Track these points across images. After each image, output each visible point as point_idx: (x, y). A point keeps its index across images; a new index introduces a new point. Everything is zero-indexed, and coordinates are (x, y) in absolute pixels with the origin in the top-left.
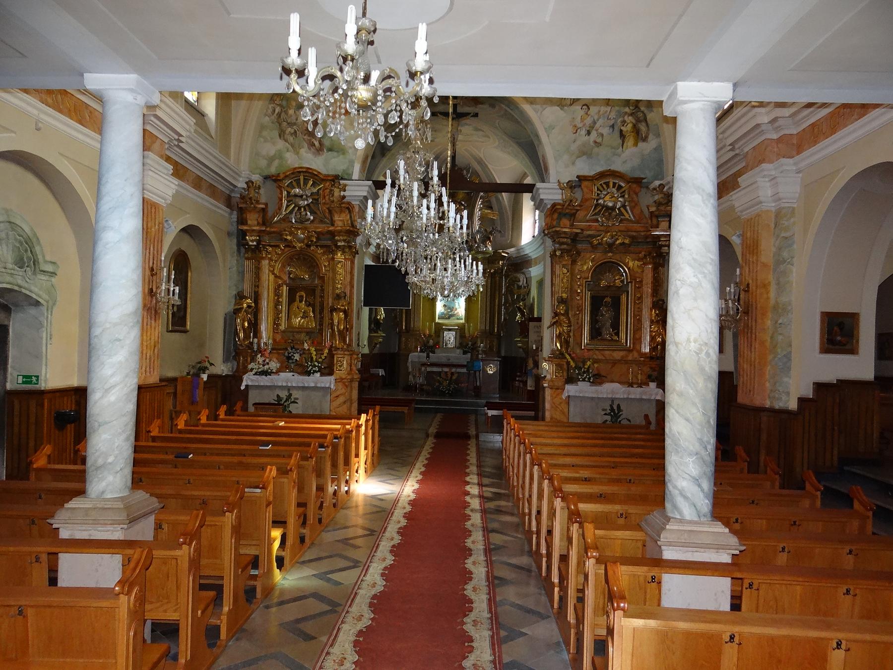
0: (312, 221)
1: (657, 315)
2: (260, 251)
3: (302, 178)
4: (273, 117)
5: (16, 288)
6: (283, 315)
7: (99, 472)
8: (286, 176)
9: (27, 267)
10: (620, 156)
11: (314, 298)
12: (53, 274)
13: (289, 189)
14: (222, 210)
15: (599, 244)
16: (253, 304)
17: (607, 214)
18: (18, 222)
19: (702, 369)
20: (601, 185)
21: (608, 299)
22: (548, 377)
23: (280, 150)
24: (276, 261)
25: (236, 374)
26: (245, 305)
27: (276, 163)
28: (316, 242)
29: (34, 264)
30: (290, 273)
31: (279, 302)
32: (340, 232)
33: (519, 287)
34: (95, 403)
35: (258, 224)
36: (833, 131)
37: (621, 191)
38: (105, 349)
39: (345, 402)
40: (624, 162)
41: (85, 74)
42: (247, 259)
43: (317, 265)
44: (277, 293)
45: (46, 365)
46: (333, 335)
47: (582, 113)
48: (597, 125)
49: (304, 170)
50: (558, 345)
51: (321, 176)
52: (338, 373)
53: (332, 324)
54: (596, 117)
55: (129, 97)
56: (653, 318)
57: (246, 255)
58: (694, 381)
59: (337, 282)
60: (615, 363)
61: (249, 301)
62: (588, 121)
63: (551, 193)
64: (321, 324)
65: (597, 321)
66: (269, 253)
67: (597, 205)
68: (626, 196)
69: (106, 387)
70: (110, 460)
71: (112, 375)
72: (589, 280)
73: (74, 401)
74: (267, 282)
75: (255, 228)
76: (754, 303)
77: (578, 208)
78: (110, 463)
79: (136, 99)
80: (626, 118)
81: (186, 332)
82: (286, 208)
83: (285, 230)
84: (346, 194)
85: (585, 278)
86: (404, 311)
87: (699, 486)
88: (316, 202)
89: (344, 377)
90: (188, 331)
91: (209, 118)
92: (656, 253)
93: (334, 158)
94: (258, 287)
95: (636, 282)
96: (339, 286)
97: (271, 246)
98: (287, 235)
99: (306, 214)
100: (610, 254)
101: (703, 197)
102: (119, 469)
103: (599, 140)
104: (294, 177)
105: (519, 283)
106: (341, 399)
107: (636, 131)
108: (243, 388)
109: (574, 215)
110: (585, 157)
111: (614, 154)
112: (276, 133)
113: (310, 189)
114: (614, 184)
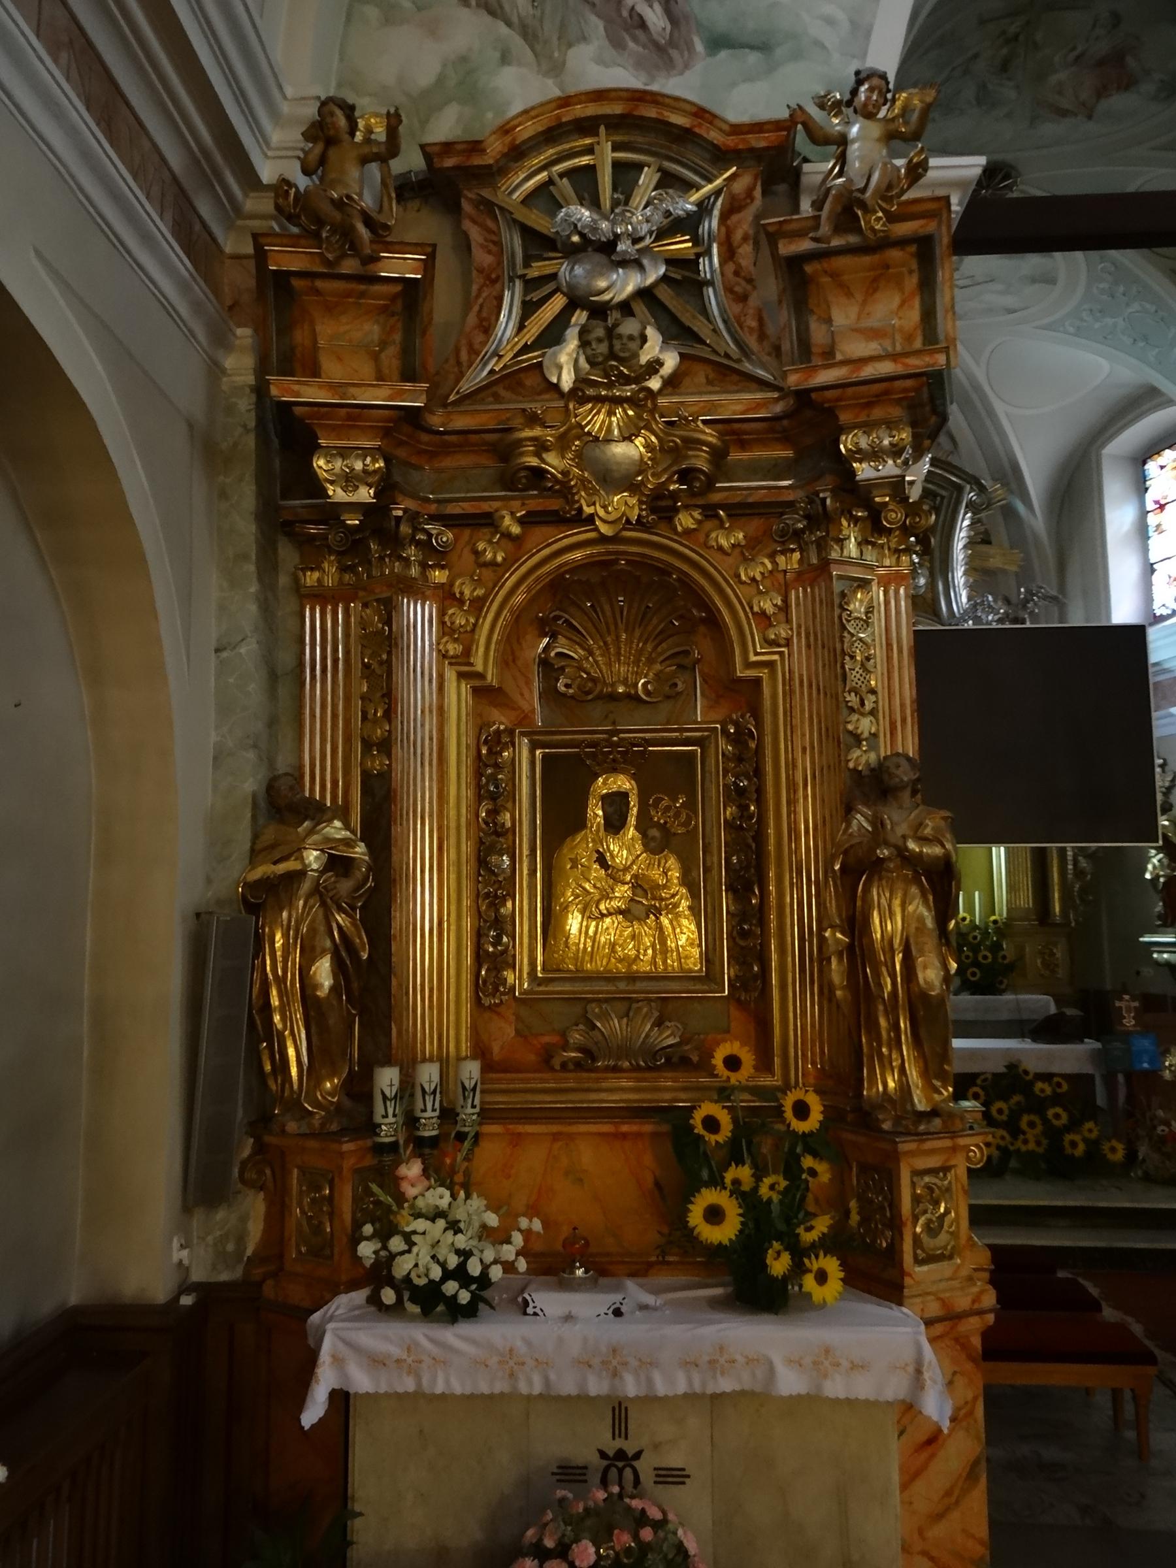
11: (690, 805)
16: (360, 850)
23: (464, 59)
26: (313, 857)
31: (500, 832)
42: (321, 597)
49: (617, 109)
51: (714, 136)
57: (311, 578)
59: (852, 699)
61: (336, 829)
74: (430, 724)
86: (1055, 852)
93: (749, 79)
94: (386, 746)
96: (865, 725)
98: (541, 447)
108: (312, 1414)
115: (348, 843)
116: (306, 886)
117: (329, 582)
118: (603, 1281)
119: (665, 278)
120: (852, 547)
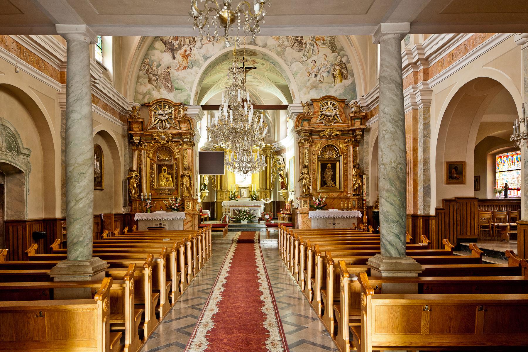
0: (169, 129)
1: (356, 172)
2: (141, 145)
3: (162, 104)
4: (144, 71)
5: (8, 162)
6: (155, 180)
7: (75, 246)
8: (154, 104)
9: (14, 150)
10: (333, 88)
11: (172, 170)
12: (28, 155)
13: (155, 111)
14: (119, 123)
15: (324, 136)
16: (138, 175)
17: (328, 119)
18: (7, 125)
19: (399, 177)
20: (324, 103)
21: (329, 165)
22: (299, 208)
23: (149, 90)
24: (150, 151)
25: (131, 213)
26: (134, 175)
27: (147, 97)
28: (172, 140)
29: (17, 149)
30: (158, 157)
32: (185, 133)
33: (280, 164)
34: (71, 208)
35: (140, 130)
36: (450, 63)
37: (335, 106)
38: (76, 179)
39: (191, 226)
40: (335, 91)
41: (56, 25)
42: (135, 150)
43: (173, 152)
44: (152, 169)
45: (27, 206)
46: (183, 190)
47: (312, 65)
48: (320, 71)
49: (164, 100)
50: (304, 190)
52: (187, 211)
53: (183, 184)
54: (320, 67)
55: (82, 38)
56: (354, 174)
57: (133, 148)
58: (394, 183)
59: (184, 161)
60: (334, 199)
62: (316, 69)
63: (297, 108)
64: (176, 184)
65: (324, 177)
66: (146, 146)
67: (322, 115)
68: (337, 109)
69: (77, 199)
70: (81, 239)
71: (80, 193)
72: (319, 155)
73: (43, 226)
75: (138, 132)
76: (410, 160)
77: (312, 116)
78: (81, 241)
79: (86, 39)
80: (336, 67)
81: (102, 190)
82: (155, 121)
83: (154, 133)
84: (188, 113)
85: (317, 154)
87: (399, 239)
88: (170, 118)
89: (190, 212)
90: (103, 190)
91: (110, 73)
92: (354, 139)
94: (141, 165)
95: (344, 155)
97: (147, 142)
98: (155, 136)
99: (166, 125)
100: (330, 141)
101: (396, 86)
102: (86, 244)
103: (322, 80)
104: (158, 104)
105: (279, 162)
106: (189, 224)
107: (341, 74)
109: (310, 120)
110: (314, 89)
111: (330, 87)
112: (146, 80)
113: (167, 111)
114: (331, 103)
115: (137, 174)
116: (133, 178)
117: (135, 148)
118: (93, 139)
119: (168, 118)
120: (185, 146)
